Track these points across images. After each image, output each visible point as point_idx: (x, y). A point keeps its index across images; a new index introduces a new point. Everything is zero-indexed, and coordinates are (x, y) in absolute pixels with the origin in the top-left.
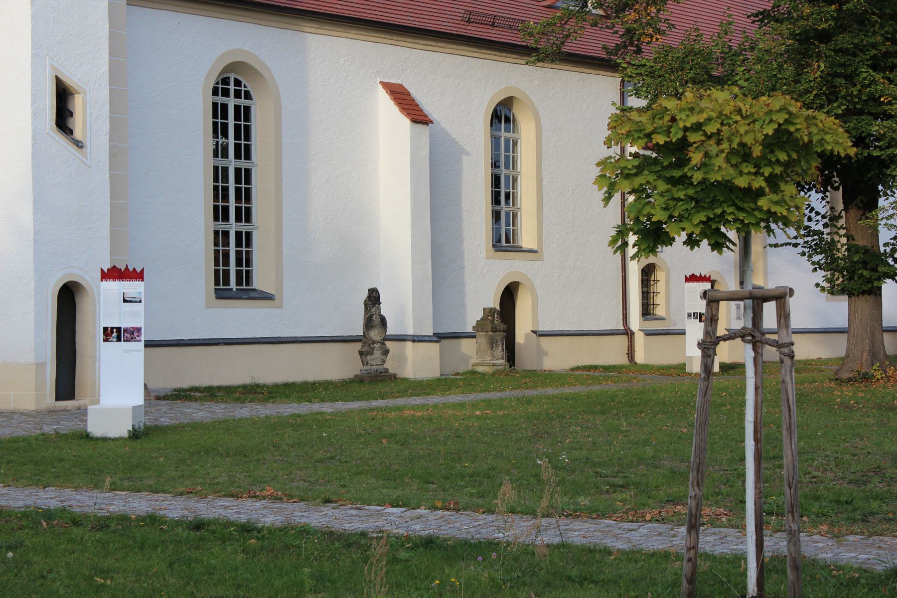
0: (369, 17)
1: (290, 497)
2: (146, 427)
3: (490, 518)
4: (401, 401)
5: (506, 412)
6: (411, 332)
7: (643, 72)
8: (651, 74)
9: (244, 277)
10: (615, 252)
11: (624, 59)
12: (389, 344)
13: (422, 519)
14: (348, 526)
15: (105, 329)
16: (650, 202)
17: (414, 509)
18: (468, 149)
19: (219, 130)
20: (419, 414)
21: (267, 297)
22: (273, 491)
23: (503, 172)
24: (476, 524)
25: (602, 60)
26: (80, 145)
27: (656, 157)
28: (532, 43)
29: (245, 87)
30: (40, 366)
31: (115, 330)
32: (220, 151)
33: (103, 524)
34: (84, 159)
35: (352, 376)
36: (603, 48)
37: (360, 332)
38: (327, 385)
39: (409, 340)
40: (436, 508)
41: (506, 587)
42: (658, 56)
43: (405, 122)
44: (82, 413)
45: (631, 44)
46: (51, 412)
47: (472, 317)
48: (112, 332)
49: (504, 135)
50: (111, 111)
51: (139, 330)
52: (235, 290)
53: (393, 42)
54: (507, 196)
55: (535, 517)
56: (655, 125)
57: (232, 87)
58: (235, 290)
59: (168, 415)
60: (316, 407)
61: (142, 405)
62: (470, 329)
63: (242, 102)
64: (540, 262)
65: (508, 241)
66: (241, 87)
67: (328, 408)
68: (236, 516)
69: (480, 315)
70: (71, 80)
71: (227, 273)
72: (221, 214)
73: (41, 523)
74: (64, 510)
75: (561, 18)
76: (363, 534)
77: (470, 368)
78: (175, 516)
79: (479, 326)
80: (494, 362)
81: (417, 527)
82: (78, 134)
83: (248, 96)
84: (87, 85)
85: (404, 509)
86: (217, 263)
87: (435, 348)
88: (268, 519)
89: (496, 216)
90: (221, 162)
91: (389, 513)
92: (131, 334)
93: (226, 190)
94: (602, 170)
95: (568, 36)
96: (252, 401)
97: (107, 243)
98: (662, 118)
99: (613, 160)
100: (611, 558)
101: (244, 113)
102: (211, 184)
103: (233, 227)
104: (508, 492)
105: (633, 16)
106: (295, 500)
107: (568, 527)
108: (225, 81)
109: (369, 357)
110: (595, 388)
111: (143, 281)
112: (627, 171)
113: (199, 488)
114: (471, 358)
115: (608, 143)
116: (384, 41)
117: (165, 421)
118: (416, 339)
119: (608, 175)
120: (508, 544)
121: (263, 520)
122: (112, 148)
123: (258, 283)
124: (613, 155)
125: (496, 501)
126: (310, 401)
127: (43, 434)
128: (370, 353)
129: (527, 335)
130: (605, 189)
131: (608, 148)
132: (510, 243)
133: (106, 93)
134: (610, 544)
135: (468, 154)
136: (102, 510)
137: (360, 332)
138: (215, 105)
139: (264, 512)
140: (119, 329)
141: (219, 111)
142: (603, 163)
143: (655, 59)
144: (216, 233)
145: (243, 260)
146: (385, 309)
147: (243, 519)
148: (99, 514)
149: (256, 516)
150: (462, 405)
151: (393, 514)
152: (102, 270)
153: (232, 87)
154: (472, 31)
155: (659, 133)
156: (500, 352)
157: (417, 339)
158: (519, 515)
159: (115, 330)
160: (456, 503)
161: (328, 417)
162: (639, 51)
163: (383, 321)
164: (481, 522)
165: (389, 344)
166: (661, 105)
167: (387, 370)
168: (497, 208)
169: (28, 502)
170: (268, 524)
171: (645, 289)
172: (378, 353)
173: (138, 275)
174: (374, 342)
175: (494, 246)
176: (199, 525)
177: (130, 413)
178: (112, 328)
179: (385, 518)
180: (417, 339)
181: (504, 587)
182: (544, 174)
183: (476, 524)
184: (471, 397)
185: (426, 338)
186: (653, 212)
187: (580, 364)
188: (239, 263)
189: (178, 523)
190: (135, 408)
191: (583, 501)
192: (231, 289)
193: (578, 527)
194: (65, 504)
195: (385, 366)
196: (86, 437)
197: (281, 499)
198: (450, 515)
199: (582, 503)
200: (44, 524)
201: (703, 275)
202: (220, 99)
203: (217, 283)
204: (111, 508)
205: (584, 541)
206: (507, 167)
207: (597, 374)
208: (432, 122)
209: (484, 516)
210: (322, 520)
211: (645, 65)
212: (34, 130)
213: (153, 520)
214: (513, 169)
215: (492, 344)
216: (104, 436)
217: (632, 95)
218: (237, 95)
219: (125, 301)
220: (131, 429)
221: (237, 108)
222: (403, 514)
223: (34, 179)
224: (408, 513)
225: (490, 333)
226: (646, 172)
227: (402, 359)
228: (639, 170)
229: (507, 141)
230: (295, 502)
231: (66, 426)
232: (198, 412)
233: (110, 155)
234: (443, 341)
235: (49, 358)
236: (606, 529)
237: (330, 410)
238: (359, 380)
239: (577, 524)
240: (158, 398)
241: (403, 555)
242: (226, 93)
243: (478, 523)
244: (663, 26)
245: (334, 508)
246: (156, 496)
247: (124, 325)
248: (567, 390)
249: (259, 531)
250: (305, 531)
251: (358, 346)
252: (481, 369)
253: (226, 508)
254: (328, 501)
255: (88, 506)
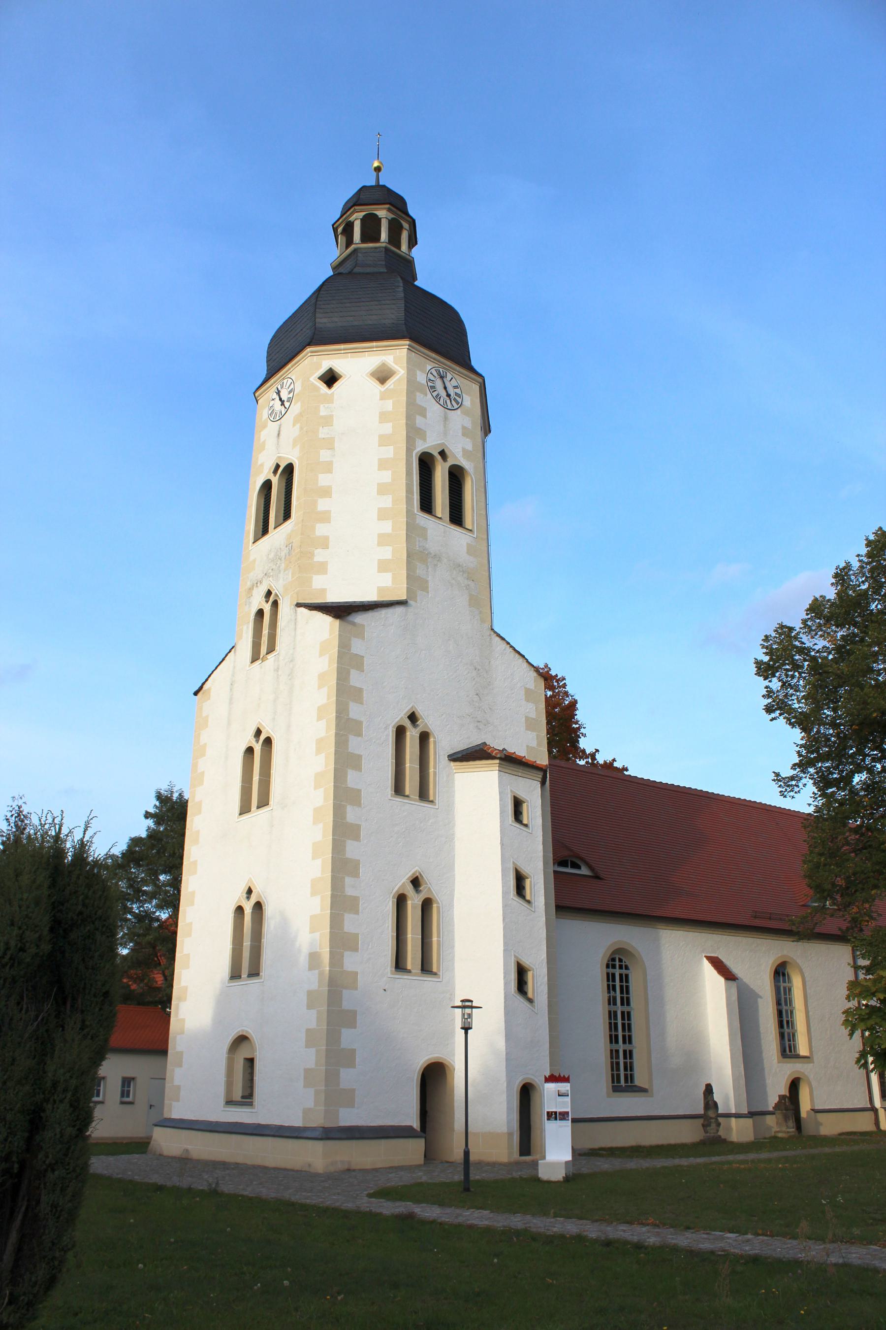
0: (696, 918)
1: (664, 1224)
2: (573, 1174)
3: (795, 1242)
4: (730, 1157)
5: (799, 1165)
6: (733, 1111)
7: (865, 943)
8: (870, 944)
9: (630, 1078)
10: (860, 1068)
11: (852, 935)
12: (720, 1120)
13: (750, 1242)
14: (701, 1246)
15: (548, 1113)
16: (879, 1035)
17: (744, 1234)
18: (760, 994)
19: (611, 988)
20: (743, 1166)
21: (643, 1090)
22: (653, 1220)
23: (784, 1008)
24: (786, 1246)
25: (838, 936)
26: (531, 1001)
27: (880, 1006)
28: (794, 928)
29: (625, 962)
30: (510, 1134)
31: (553, 1113)
32: (612, 1001)
33: (551, 1240)
34: (533, 1009)
35: (698, 1141)
36: (839, 930)
37: (701, 1111)
38: (683, 1146)
39: (733, 1117)
40: (758, 1235)
41: (810, 1295)
42: (873, 933)
43: (722, 980)
44: (535, 1165)
45: (856, 926)
46: (517, 1163)
47: (772, 1100)
48: (552, 1115)
49: (782, 985)
50: (549, 980)
51: (567, 1113)
52: (624, 1086)
53: (711, 932)
54: (788, 1022)
55: (824, 1242)
56: (877, 987)
57: (617, 963)
58: (624, 1086)
59: (587, 1167)
60: (677, 1161)
61: (570, 1161)
62: (771, 1109)
63: (624, 971)
64: (812, 1064)
65: (790, 1051)
66: (622, 962)
67: (684, 1162)
68: (631, 1237)
69: (776, 1099)
70: (526, 962)
71: (618, 1076)
72: (613, 1039)
73: (513, 1238)
74: (526, 1230)
75: (811, 914)
76: (712, 1252)
77: (773, 1134)
78: (593, 1236)
79: (777, 1106)
80: (788, 1130)
81: (747, 1248)
82: (530, 995)
83: (627, 968)
84: (534, 966)
85: (738, 1235)
86: (612, 1070)
87: (749, 1122)
88: (651, 1240)
89: (782, 1035)
90: (613, 1008)
91: (728, 1238)
92: (563, 1116)
93: (616, 1025)
94: (846, 1017)
95: (816, 924)
96: (637, 1157)
97: (548, 1059)
98: (880, 982)
99: (852, 1010)
100: (880, 1275)
101: (625, 978)
102: (607, 1021)
103: (621, 1047)
104: (804, 1226)
105: (855, 910)
106: (667, 1227)
107: (847, 1251)
108: (613, 960)
109: (708, 1128)
110: (856, 1148)
111: (569, 1083)
112: (862, 1017)
113: (607, 1217)
114: (773, 1127)
115: (848, 998)
116: (705, 931)
117: (585, 1170)
118: (737, 1116)
119: (850, 1019)
120: (808, 1262)
121: (648, 1240)
122: (549, 1002)
123: (639, 1081)
124: (852, 1007)
125: (797, 1230)
126: (673, 1158)
127: (512, 1178)
128: (709, 1125)
129: (808, 1112)
130: (850, 1028)
131: (849, 1001)
132: (792, 1052)
133: (545, 970)
134: (877, 1265)
135: (761, 997)
136: (549, 1230)
137: (701, 1111)
138: (608, 974)
139: (649, 1235)
140: (556, 1113)
141: (610, 977)
142: (846, 1012)
143: (872, 935)
144: (611, 1051)
145: (629, 1067)
146: (716, 1097)
147: (635, 1239)
148: (548, 1234)
149: (643, 1237)
150: (769, 1160)
151: (730, 1238)
152: (545, 1077)
153: (617, 963)
154: (757, 922)
155: (879, 992)
156: (791, 1123)
157: (737, 1116)
158: (814, 1241)
159: (553, 1113)
160: (771, 1232)
161: (685, 1168)
162: (861, 930)
163: (716, 1104)
164: (789, 1246)
165: (720, 1120)
166: (879, 974)
167: (720, 1136)
168: (782, 1030)
169: (505, 1224)
170: (651, 1244)
171: (882, 1080)
172: (713, 1125)
173: (566, 1080)
174: (711, 1118)
175: (782, 1055)
176: (608, 1243)
177: (564, 1165)
178: (552, 1112)
179: (725, 1241)
180: (737, 1116)
181: (808, 1295)
182: (809, 1008)
183: (786, 1246)
184: (775, 1155)
185: (744, 1115)
186: (881, 1042)
187: (844, 1131)
188: (626, 1069)
189: (596, 1241)
190: (567, 1163)
191: (856, 1231)
192: (622, 1086)
193: (855, 1251)
194: (528, 1225)
195: (719, 1133)
196: (538, 1180)
197: (658, 1226)
198: (768, 1240)
199: (855, 1233)
200: (515, 1239)
201: (562, 1076)
202: (611, 970)
203: (613, 1082)
204: (555, 1229)
205: (859, 1262)
206: (786, 1004)
207: (856, 1137)
208: (737, 979)
209: (790, 1241)
210: (685, 1241)
211: (865, 939)
212: (505, 993)
213: (580, 1238)
214: (790, 1006)
215: (786, 1118)
216: (549, 1180)
217: (859, 958)
218: (621, 967)
219: (559, 1095)
220: (564, 1176)
221: (621, 975)
222: (737, 1238)
223: (506, 1022)
224: (740, 1238)
225: (784, 1111)
226: (874, 1017)
227: (729, 1129)
228: (870, 1016)
229: (785, 988)
230: (667, 1228)
231: (526, 1173)
232: (605, 1165)
233: (548, 1006)
234: (754, 1117)
235: (515, 1129)
236: (874, 1253)
237: (686, 1164)
238: (702, 1143)
239: (853, 1249)
240: (580, 1155)
241: (739, 1268)
242: (614, 967)
243: (787, 1246)
244: (875, 915)
245: (692, 1233)
246: (582, 1222)
247: (558, 1110)
248: (837, 1149)
249: (646, 1248)
250: (675, 1249)
251: (701, 1121)
252: (780, 1135)
253: (624, 1231)
254: (688, 1228)
255: (540, 1227)
